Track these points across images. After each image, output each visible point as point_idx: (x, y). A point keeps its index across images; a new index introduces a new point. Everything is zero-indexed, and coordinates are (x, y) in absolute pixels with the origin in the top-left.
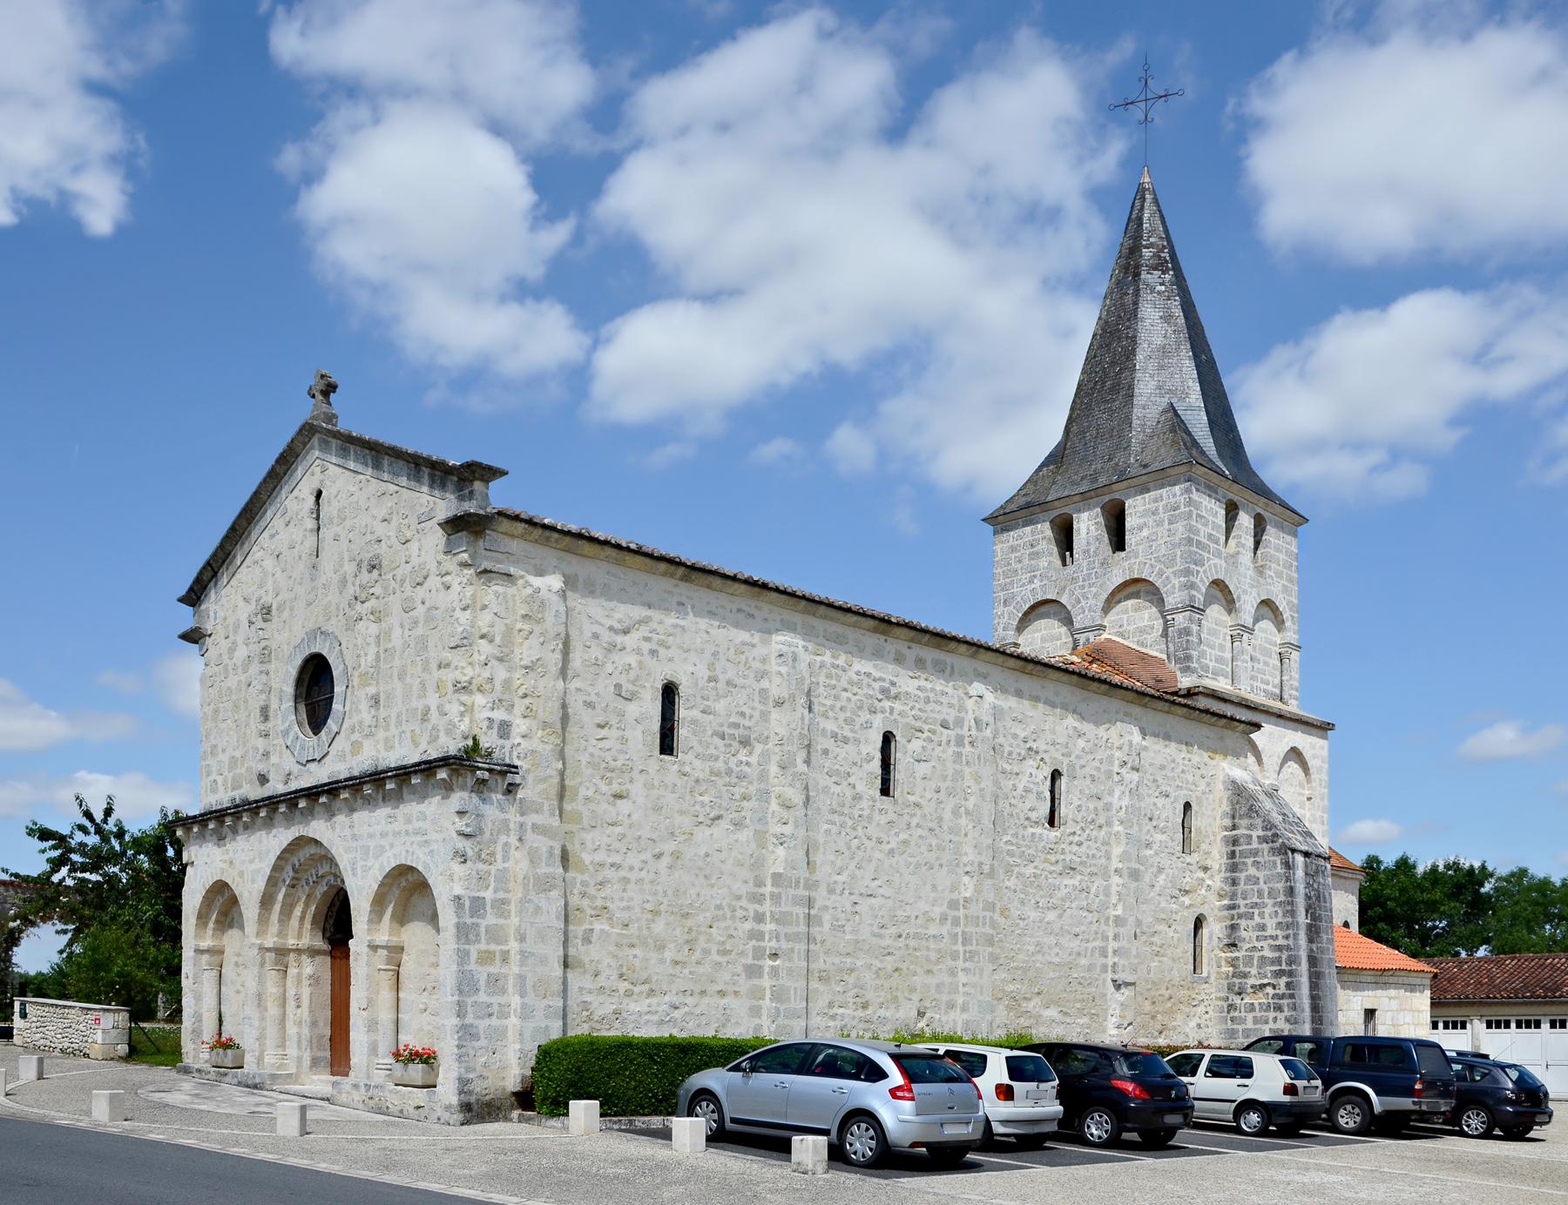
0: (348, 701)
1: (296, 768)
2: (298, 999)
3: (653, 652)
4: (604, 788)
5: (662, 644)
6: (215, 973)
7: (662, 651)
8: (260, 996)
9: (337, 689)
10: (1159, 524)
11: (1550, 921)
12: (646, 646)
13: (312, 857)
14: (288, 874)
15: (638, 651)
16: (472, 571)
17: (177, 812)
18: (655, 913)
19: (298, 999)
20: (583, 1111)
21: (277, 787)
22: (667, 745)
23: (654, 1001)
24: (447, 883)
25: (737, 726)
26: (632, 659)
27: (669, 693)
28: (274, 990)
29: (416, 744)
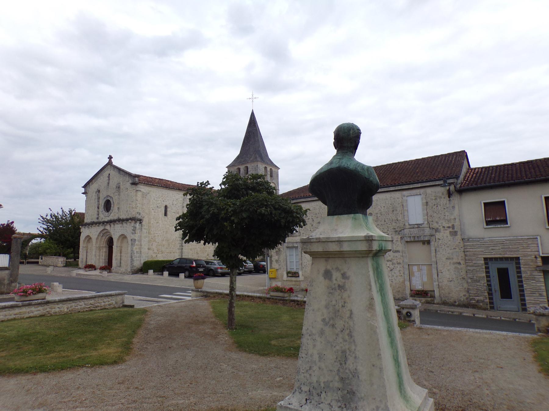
0: (114, 208)
1: (104, 217)
2: (102, 255)
3: (163, 201)
4: (155, 222)
5: (165, 199)
6: (86, 251)
7: (165, 201)
8: (95, 255)
9: (112, 206)
10: (253, 171)
11: (192, 267)
12: (162, 200)
13: (106, 232)
14: (102, 235)
15: (161, 201)
16: (135, 190)
17: (70, 212)
18: (163, 240)
19: (102, 255)
20: (151, 272)
21: (100, 220)
22: (166, 214)
23: (163, 254)
24: (130, 236)
25: (177, 211)
26: (160, 202)
27: (166, 207)
28: (98, 254)
29: (125, 216)
